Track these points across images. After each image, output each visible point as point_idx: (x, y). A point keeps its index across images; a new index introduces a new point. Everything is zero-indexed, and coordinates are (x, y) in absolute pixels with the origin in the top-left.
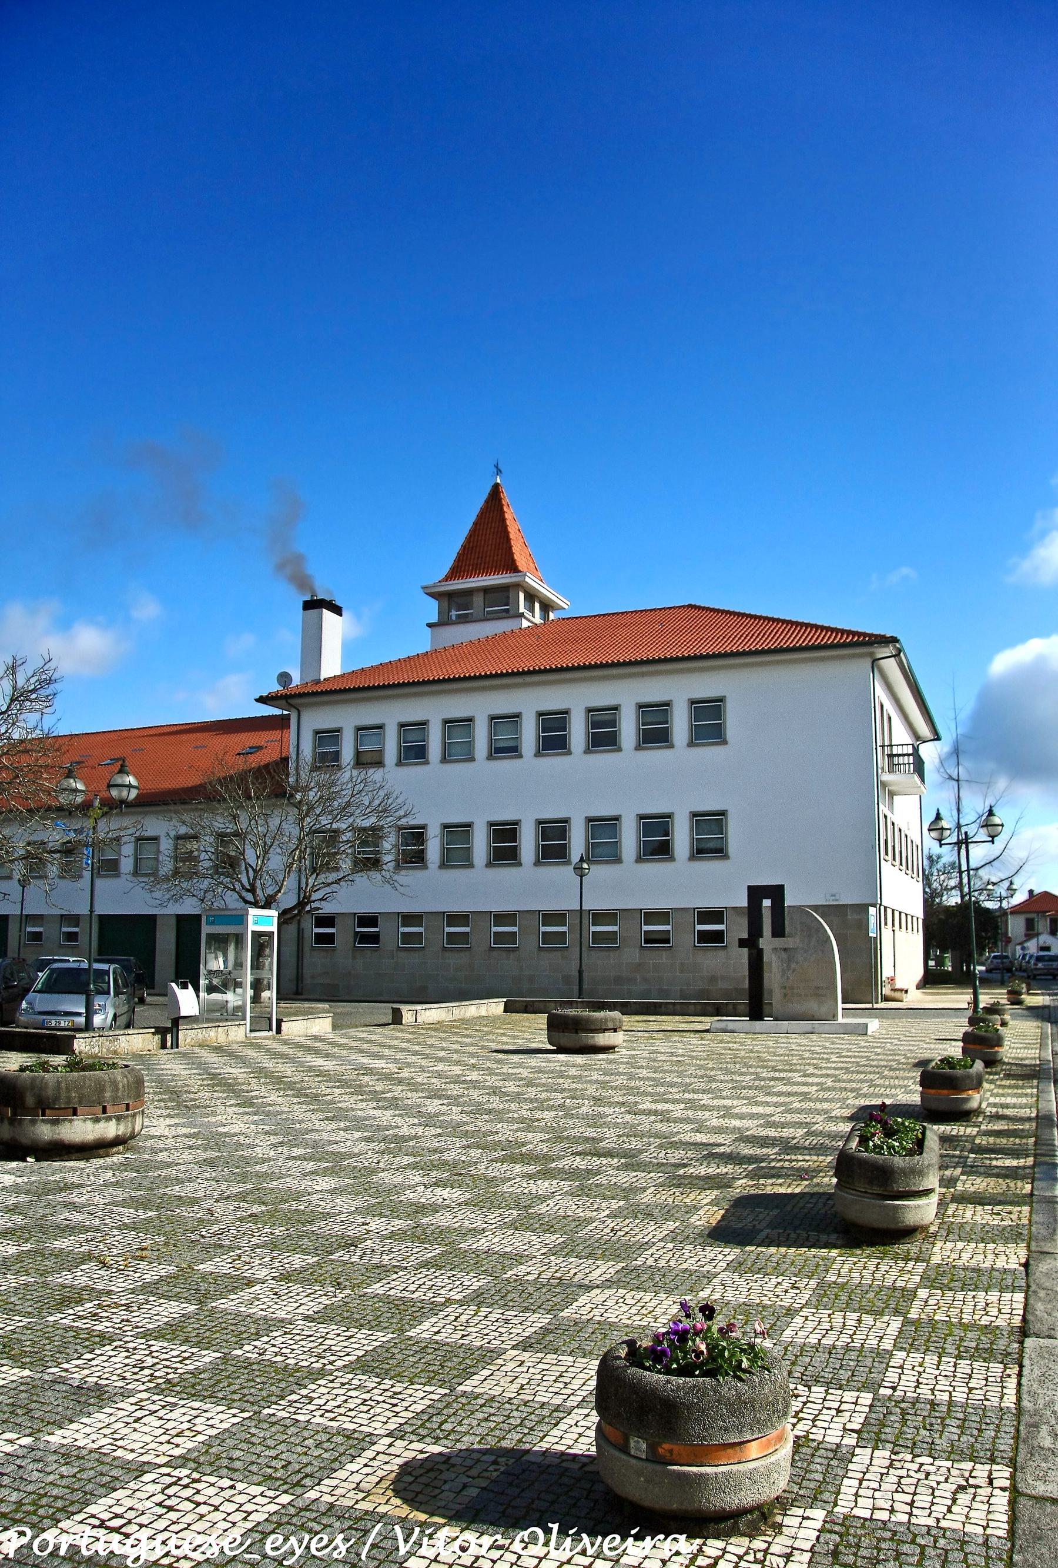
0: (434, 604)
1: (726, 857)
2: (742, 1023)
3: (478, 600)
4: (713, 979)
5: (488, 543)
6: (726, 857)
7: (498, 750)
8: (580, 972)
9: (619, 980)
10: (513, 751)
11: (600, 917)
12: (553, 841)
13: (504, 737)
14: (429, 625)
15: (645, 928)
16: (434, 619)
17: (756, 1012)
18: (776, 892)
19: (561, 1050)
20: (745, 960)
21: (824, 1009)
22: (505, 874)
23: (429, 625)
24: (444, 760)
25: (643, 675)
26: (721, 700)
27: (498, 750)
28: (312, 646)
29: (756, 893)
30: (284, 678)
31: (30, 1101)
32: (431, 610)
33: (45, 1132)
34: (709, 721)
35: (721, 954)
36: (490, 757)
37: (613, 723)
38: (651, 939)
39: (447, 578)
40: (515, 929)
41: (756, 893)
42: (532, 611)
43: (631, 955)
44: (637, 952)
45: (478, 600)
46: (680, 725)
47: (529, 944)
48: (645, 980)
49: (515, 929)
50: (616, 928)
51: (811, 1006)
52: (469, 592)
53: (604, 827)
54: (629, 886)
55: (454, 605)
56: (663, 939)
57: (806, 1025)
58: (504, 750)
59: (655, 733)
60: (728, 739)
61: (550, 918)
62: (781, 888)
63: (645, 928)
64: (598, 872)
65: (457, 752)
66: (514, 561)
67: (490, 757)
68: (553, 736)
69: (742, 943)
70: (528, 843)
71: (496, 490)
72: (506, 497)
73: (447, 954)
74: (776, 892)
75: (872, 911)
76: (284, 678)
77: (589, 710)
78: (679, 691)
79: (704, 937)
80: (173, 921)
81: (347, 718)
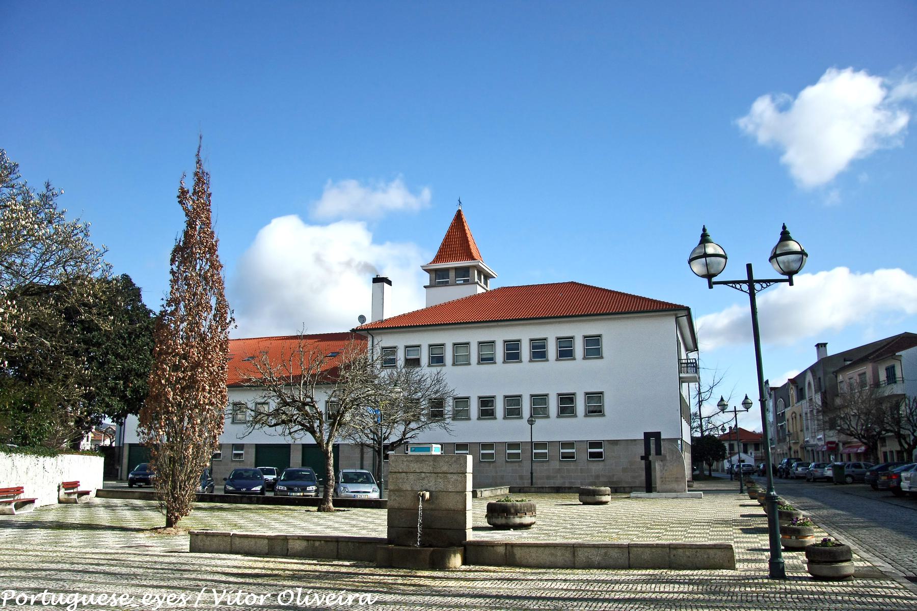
0: (427, 275)
1: (603, 415)
2: (644, 494)
3: (452, 274)
4: (597, 477)
5: (457, 242)
6: (603, 415)
7: (483, 360)
8: (532, 473)
9: (548, 477)
10: (490, 360)
11: (543, 445)
12: (513, 407)
13: (486, 352)
14: (425, 287)
15: (562, 451)
16: (428, 284)
17: (650, 487)
18: (657, 435)
19: (584, 504)
20: (644, 466)
21: (680, 487)
22: (487, 423)
23: (425, 287)
24: (454, 364)
25: (559, 322)
26: (600, 336)
27: (483, 360)
28: (378, 302)
29: (647, 435)
30: (362, 318)
31: (513, 511)
32: (426, 279)
33: (517, 520)
34: (594, 346)
35: (601, 464)
36: (479, 363)
37: (544, 347)
38: (565, 456)
39: (434, 262)
40: (519, 451)
41: (647, 435)
42: (480, 280)
43: (555, 465)
44: (558, 463)
45: (452, 274)
46: (579, 348)
47: (500, 459)
48: (562, 477)
49: (519, 451)
50: (546, 451)
51: (674, 486)
52: (447, 270)
53: (539, 400)
54: (553, 429)
55: (438, 277)
56: (571, 456)
57: (674, 494)
58: (487, 360)
59: (566, 352)
60: (604, 355)
61: (512, 445)
62: (659, 433)
63: (562, 451)
64: (539, 423)
65: (461, 360)
66: (471, 253)
67: (479, 363)
68: (512, 352)
69: (642, 458)
70: (499, 408)
71: (459, 214)
72: (465, 217)
73: (508, 465)
74: (657, 435)
75: (679, 442)
76: (362, 318)
77: (531, 340)
78: (578, 331)
79: (592, 455)
80: (301, 447)
81: (400, 341)
